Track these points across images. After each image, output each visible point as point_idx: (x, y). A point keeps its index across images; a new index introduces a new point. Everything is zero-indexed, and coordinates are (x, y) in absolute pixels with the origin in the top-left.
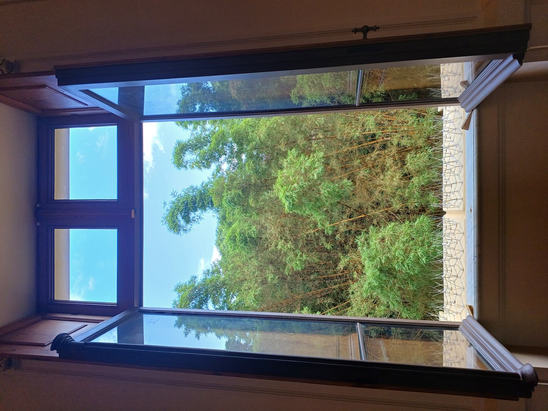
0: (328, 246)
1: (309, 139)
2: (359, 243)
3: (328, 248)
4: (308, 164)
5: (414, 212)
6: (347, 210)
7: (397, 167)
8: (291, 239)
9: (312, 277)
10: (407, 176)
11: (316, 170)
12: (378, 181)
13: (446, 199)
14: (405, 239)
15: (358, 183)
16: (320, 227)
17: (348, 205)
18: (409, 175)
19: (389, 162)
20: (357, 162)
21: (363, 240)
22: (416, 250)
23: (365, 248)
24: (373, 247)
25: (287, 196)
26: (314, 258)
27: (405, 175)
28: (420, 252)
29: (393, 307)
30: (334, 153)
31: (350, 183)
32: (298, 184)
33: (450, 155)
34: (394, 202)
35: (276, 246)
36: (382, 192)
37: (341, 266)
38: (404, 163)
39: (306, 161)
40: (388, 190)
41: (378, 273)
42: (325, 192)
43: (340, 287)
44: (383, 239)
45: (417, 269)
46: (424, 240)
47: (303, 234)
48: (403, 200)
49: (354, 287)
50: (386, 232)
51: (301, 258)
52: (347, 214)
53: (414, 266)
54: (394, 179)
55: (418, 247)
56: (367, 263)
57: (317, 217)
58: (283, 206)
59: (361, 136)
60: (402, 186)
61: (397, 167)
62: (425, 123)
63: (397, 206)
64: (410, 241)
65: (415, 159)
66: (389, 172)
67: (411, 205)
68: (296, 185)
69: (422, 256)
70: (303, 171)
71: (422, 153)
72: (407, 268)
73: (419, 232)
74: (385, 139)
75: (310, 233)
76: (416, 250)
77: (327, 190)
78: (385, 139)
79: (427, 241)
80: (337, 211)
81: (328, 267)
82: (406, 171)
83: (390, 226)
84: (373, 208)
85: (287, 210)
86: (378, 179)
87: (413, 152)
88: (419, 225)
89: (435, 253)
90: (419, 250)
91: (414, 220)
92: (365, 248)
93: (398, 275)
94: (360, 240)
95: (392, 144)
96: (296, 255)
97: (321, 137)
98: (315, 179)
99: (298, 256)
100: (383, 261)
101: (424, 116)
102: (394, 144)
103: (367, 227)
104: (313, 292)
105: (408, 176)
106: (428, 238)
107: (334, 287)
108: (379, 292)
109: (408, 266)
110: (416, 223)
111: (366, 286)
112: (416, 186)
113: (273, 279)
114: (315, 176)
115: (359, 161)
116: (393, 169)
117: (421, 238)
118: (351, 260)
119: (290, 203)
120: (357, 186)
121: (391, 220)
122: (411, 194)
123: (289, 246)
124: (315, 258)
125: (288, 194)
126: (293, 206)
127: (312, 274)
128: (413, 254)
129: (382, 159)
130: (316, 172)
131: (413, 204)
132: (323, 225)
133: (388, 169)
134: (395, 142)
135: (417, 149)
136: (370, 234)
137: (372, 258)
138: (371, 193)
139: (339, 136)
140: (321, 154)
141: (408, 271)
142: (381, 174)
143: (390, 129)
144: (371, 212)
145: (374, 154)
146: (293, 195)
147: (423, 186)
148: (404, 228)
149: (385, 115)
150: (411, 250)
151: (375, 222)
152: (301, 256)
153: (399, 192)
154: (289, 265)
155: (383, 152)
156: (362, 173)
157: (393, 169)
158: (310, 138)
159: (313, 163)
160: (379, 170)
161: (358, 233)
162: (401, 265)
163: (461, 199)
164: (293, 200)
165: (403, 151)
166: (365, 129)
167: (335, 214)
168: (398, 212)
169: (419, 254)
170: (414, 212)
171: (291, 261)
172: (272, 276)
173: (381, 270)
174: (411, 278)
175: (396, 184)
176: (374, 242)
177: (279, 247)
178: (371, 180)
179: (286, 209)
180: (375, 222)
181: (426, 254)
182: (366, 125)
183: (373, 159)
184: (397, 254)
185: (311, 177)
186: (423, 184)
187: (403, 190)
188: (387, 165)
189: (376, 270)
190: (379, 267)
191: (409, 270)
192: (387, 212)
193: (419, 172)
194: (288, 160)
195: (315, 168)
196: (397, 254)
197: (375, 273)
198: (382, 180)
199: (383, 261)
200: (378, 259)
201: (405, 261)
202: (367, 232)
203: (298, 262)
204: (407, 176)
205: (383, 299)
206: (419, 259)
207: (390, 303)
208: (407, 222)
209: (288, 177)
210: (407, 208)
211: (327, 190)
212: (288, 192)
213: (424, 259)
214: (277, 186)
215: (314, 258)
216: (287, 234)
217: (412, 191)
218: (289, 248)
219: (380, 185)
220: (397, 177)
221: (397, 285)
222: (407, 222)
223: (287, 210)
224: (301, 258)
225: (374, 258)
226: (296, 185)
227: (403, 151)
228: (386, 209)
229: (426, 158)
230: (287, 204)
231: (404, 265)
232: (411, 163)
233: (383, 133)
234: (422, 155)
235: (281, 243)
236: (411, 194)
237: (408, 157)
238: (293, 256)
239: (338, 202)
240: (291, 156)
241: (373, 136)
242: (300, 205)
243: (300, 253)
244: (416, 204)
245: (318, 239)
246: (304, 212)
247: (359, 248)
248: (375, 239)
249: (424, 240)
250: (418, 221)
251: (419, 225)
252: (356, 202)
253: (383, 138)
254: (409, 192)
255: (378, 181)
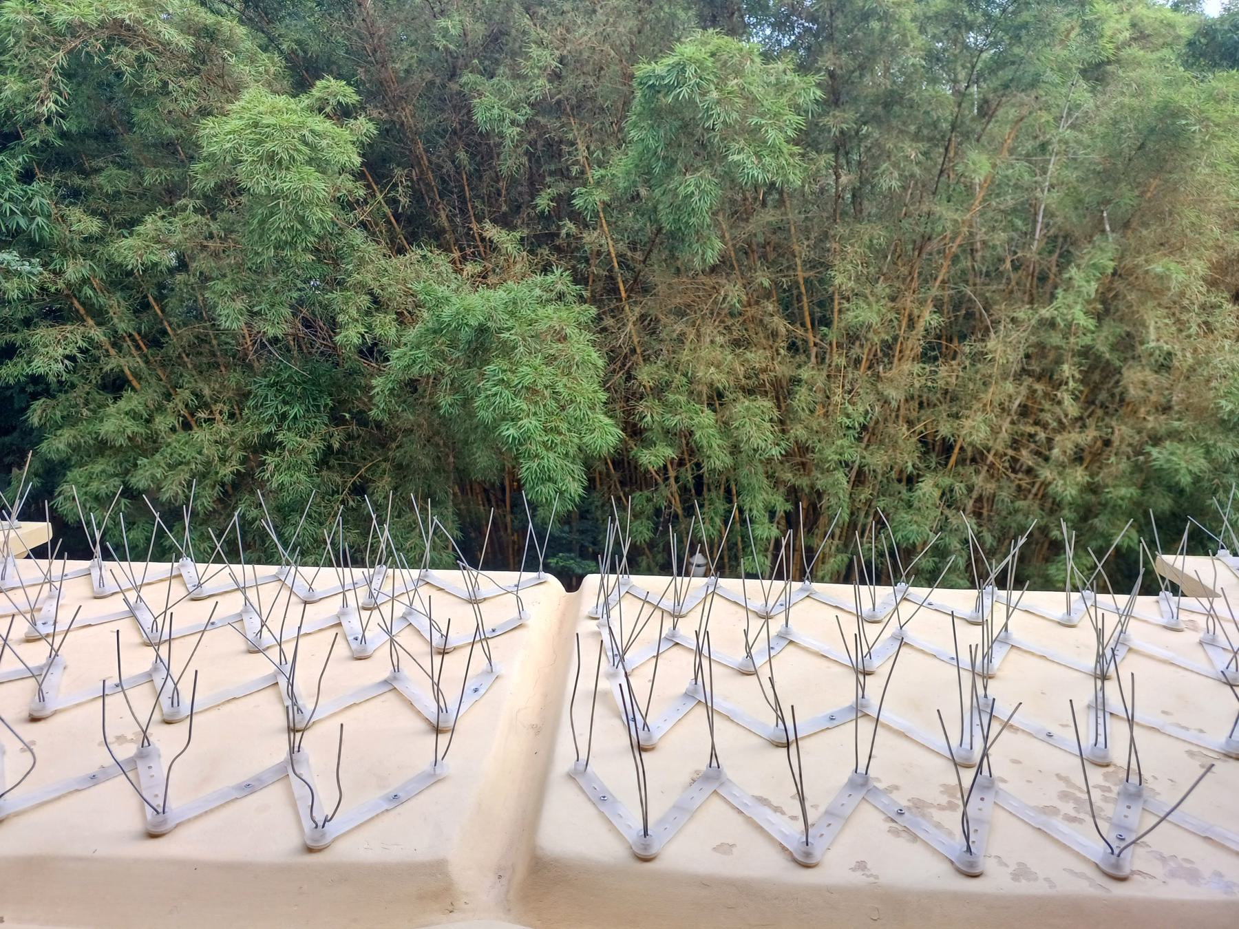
0: (543, 202)
1: (841, 146)
2: (550, 278)
3: (538, 201)
4: (772, 135)
5: (629, 413)
6: (639, 256)
7: (741, 377)
8: (560, 92)
9: (462, 155)
10: (716, 399)
11: (754, 159)
12: (708, 330)
13: (656, 607)
14: (562, 390)
15: (710, 281)
16: (594, 174)
17: (654, 255)
18: (721, 405)
19: (756, 357)
20: (763, 279)
21: (559, 287)
22: (535, 414)
23: (538, 292)
24: (541, 312)
25: (683, 70)
26: (510, 162)
27: (720, 395)
28: (529, 423)
29: (395, 356)
30: (794, 216)
31: (712, 257)
32: (718, 102)
33: (978, 668)
34: (654, 368)
35: (540, 43)
36: (681, 339)
37: (492, 232)
38: (749, 392)
39: (781, 130)
40: (685, 355)
41: (474, 323)
42: (689, 185)
43: (443, 231)
44: (564, 338)
45: (486, 415)
46: (560, 433)
47: (576, 132)
48: (659, 391)
49: (441, 261)
50: (580, 346)
51: (507, 121)
52: (629, 254)
53: (494, 409)
54: (712, 369)
55: (543, 419)
56: (499, 296)
57: (621, 166)
58: (654, 58)
59: (831, 290)
60: (694, 386)
61: (741, 377)
62: (846, 442)
63: (646, 375)
64: (557, 401)
65: (757, 419)
66: (730, 357)
67: (646, 406)
68: (715, 95)
69: (520, 428)
70: (754, 120)
71: (772, 433)
72: (489, 393)
73: (576, 424)
74: (814, 350)
75: (576, 150)
76: (535, 414)
77: (696, 193)
78: (814, 350)
79: (558, 439)
80: (636, 227)
81: (493, 200)
82: (731, 397)
83: (595, 355)
84: (643, 317)
85: (643, 69)
86: (715, 332)
87: (776, 414)
88: (597, 425)
89: (529, 456)
90: (534, 422)
91: (610, 414)
92: (538, 292)
93: (474, 372)
94: (560, 279)
95: (799, 366)
96: (515, 107)
97: (844, 179)
98: (727, 156)
99: (513, 114)
100: (506, 335)
101: (860, 439)
102: (799, 371)
103: (594, 300)
104: (425, 158)
105: (717, 402)
106: (563, 443)
107: (443, 215)
108: (430, 325)
109: (496, 394)
110: (602, 417)
111: (441, 291)
112: (692, 419)
113: (445, 32)
114: (736, 158)
115: (766, 283)
116: (737, 365)
117: (563, 427)
118: (510, 262)
119: (663, 78)
120: (702, 278)
121: (612, 360)
122: (672, 408)
123: (541, 82)
124: (509, 162)
125: (690, 71)
126: (655, 89)
127: (472, 156)
128: (525, 407)
129: (764, 341)
130: (748, 158)
131: (650, 413)
132: (598, 183)
133: (738, 356)
134: (805, 374)
135: (782, 424)
136: (574, 305)
137: (512, 309)
138: (680, 313)
139: (840, 229)
140: (796, 179)
141: (483, 395)
142: (727, 338)
143: (839, 360)
144: (632, 314)
145: (780, 324)
146: (684, 88)
147: (691, 433)
148: (589, 389)
149: (874, 349)
150: (536, 403)
151: (609, 322)
152: (513, 122)
153: (678, 379)
154: (486, 85)
155: (782, 344)
156: (733, 292)
157: (737, 365)
158: (842, 151)
159: (775, 151)
160: (735, 335)
161: (579, 279)
162: (496, 378)
163: (646, 847)
164: (670, 88)
165: (782, 392)
166: (848, 300)
167: (629, 219)
168: (629, 377)
169: (525, 421)
170: (629, 413)
171: (500, 92)
172: (453, 32)
173: (482, 330)
174: (467, 401)
175: (700, 374)
176: (552, 315)
177: (534, 51)
178: (712, 314)
179: (645, 66)
180: (609, 322)
181: (526, 438)
182: (860, 302)
183: (767, 319)
184: (525, 369)
185: (735, 146)
186: (697, 436)
187: (684, 389)
188: (748, 353)
189: (481, 318)
190: (489, 324)
191: (486, 397)
192: (633, 351)
193: (725, 427)
194: (790, 76)
195: (759, 156)
196: (525, 369)
197: (474, 316)
198: (712, 342)
199: (506, 335)
200: (509, 324)
201: (506, 388)
202: (581, 299)
203: (496, 111)
204: (716, 399)
205: (412, 333)
206: (513, 420)
207: (403, 349)
208: (603, 396)
209: (738, 73)
210: (641, 398)
211: (696, 193)
212: (696, 71)
213: (511, 431)
214: (715, 39)
215: (510, 162)
216: (574, 81)
217: (680, 411)
218: (534, 83)
219: (698, 335)
220: (716, 377)
221: (448, 368)
222: (603, 396)
223: (643, 69)
224: (507, 121)
225: (512, 314)
226: (715, 95)
227: (782, 392)
228: (638, 351)
229: (757, 441)
230: (660, 68)
231: (495, 385)
232: (748, 409)
233: (831, 344)
234: (768, 434)
235: (548, 58)
236: (672, 408)
237: (765, 404)
238: (514, 96)
239: (659, 230)
240: (802, 85)
241: (826, 322)
242: (656, 114)
243: (522, 120)
244: (649, 418)
245: (563, 174)
246: (635, 125)
247: (539, 279)
248: (560, 317)
249: (560, 433)
250: (607, 420)
251: (597, 425)
252: (658, 276)
253: (815, 345)
254: (678, 402)
255: (708, 330)
